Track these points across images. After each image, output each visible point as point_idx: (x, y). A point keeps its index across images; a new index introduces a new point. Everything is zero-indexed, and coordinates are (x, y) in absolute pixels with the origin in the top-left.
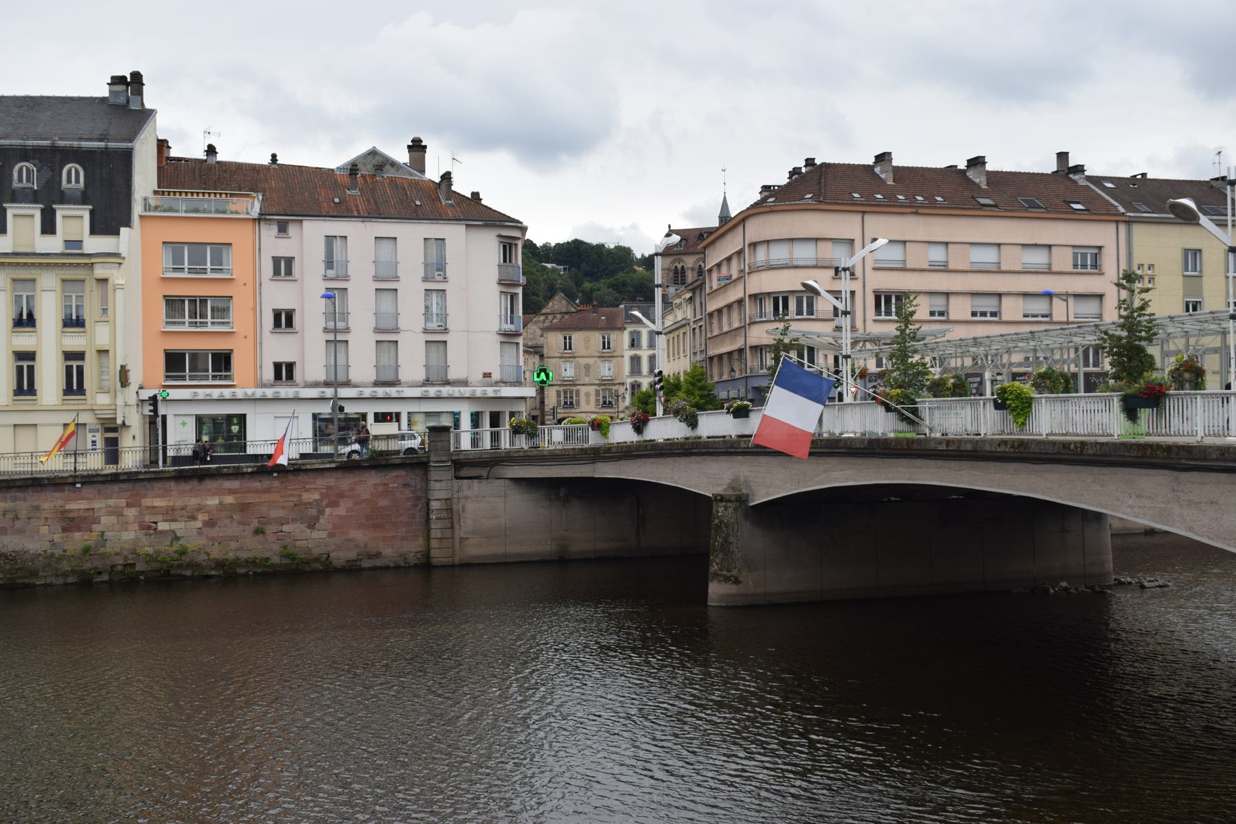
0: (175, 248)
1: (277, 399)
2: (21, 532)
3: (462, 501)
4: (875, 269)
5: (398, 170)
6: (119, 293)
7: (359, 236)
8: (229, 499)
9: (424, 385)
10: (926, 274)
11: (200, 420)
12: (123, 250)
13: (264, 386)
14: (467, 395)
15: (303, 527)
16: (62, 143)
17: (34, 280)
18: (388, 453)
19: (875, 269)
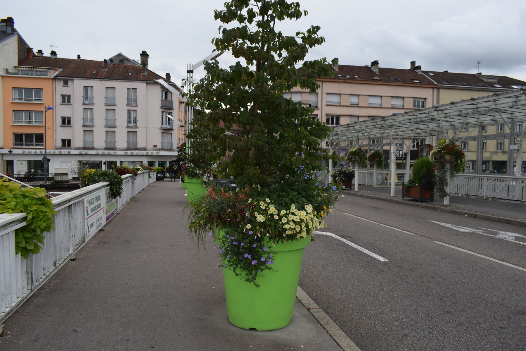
1: (60, 155)
4: (327, 105)
7: (99, 87)
9: (126, 150)
10: (349, 108)
13: (57, 149)
14: (145, 154)
18: (62, 182)
19: (327, 105)
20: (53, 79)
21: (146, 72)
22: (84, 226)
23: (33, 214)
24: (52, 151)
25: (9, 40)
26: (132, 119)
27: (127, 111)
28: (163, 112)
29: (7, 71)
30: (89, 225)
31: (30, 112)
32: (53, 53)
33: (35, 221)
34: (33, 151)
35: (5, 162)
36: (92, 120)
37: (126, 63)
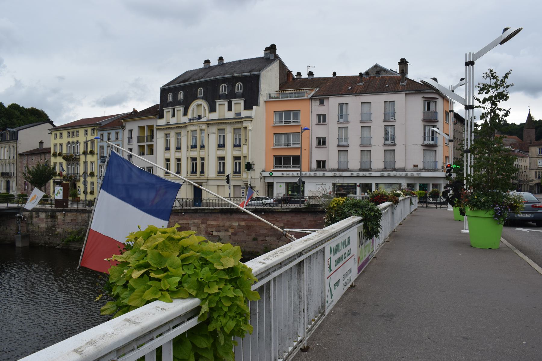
0: (279, 113)
1: (315, 177)
5: (387, 73)
6: (250, 132)
7: (353, 102)
8: (243, 223)
9: (383, 170)
11: (287, 184)
12: (253, 116)
13: (312, 171)
14: (403, 175)
15: (275, 239)
16: (236, 75)
17: (224, 129)
18: (316, 205)
20: (309, 99)
21: (406, 82)
22: (324, 288)
23: (210, 303)
24: (308, 173)
26: (390, 135)
27: (383, 127)
28: (425, 126)
29: (270, 97)
30: (332, 286)
31: (288, 134)
32: (311, 73)
33: (215, 315)
34: (291, 173)
36: (347, 139)
37: (383, 74)
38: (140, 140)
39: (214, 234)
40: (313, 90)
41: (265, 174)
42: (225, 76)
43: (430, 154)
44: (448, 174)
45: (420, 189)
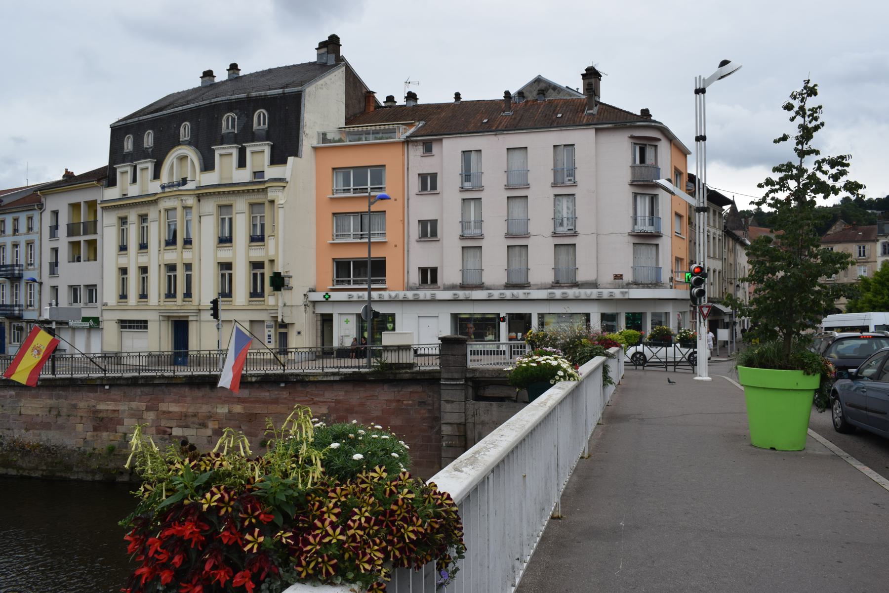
1: (416, 301)
2: (61, 428)
3: (479, 427)
5: (559, 93)
6: (281, 211)
7: (492, 148)
9: (553, 287)
12: (288, 176)
13: (411, 289)
16: (254, 94)
17: (231, 206)
18: (399, 366)
20: (403, 142)
24: (401, 295)
25: (329, 77)
28: (636, 195)
29: (324, 138)
32: (411, 96)
35: (319, 318)
36: (479, 223)
37: (552, 96)
38: (72, 230)
39: (174, 434)
40: (411, 125)
41: (314, 297)
42: (233, 97)
43: (647, 253)
44: (695, 290)
45: (627, 328)
